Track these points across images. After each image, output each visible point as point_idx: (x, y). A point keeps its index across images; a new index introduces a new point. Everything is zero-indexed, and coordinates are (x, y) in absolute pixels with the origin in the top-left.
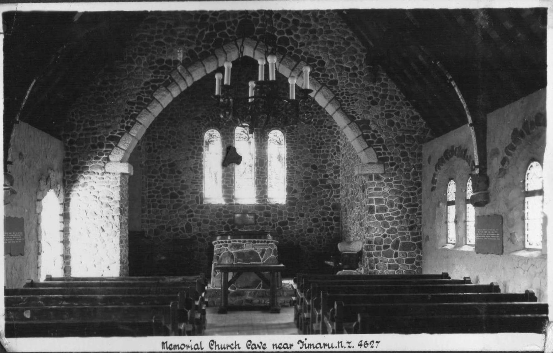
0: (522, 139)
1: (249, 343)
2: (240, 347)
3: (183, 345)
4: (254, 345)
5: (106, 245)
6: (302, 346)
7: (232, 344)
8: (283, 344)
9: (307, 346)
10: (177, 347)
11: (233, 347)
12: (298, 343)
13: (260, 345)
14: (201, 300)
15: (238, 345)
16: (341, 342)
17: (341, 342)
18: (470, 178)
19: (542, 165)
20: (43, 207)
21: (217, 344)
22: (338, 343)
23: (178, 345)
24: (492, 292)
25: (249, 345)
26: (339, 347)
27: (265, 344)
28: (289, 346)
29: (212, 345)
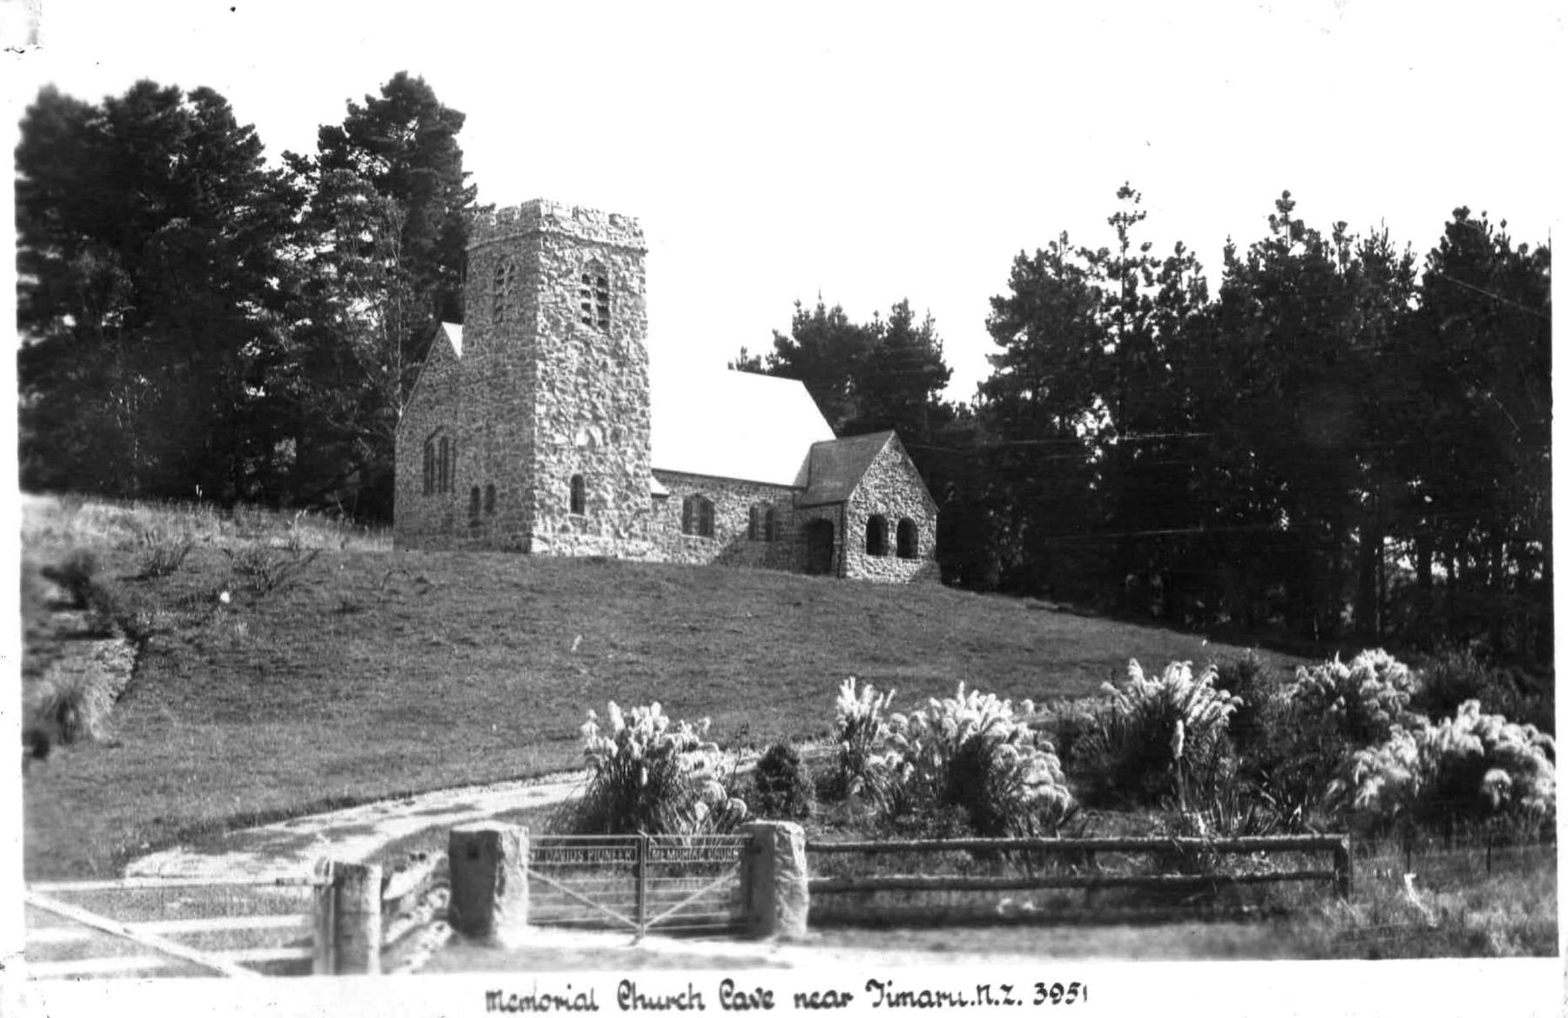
0: (791, 338)
1: (726, 988)
2: (703, 1002)
3: (547, 997)
4: (741, 995)
5: (798, 604)
6: (878, 1000)
7: (683, 996)
8: (822, 994)
9: (893, 998)
10: (908, 1000)
11: (684, 1001)
12: (868, 989)
13: (756, 996)
14: (771, 816)
15: (698, 995)
16: (987, 987)
17: (987, 987)
18: (170, 177)
19: (1554, 764)
20: (21, 114)
21: (638, 994)
22: (979, 989)
23: (911, 994)
24: (1192, 873)
25: (728, 994)
26: (980, 1003)
27: (770, 994)
28: (839, 999)
29: (626, 997)
